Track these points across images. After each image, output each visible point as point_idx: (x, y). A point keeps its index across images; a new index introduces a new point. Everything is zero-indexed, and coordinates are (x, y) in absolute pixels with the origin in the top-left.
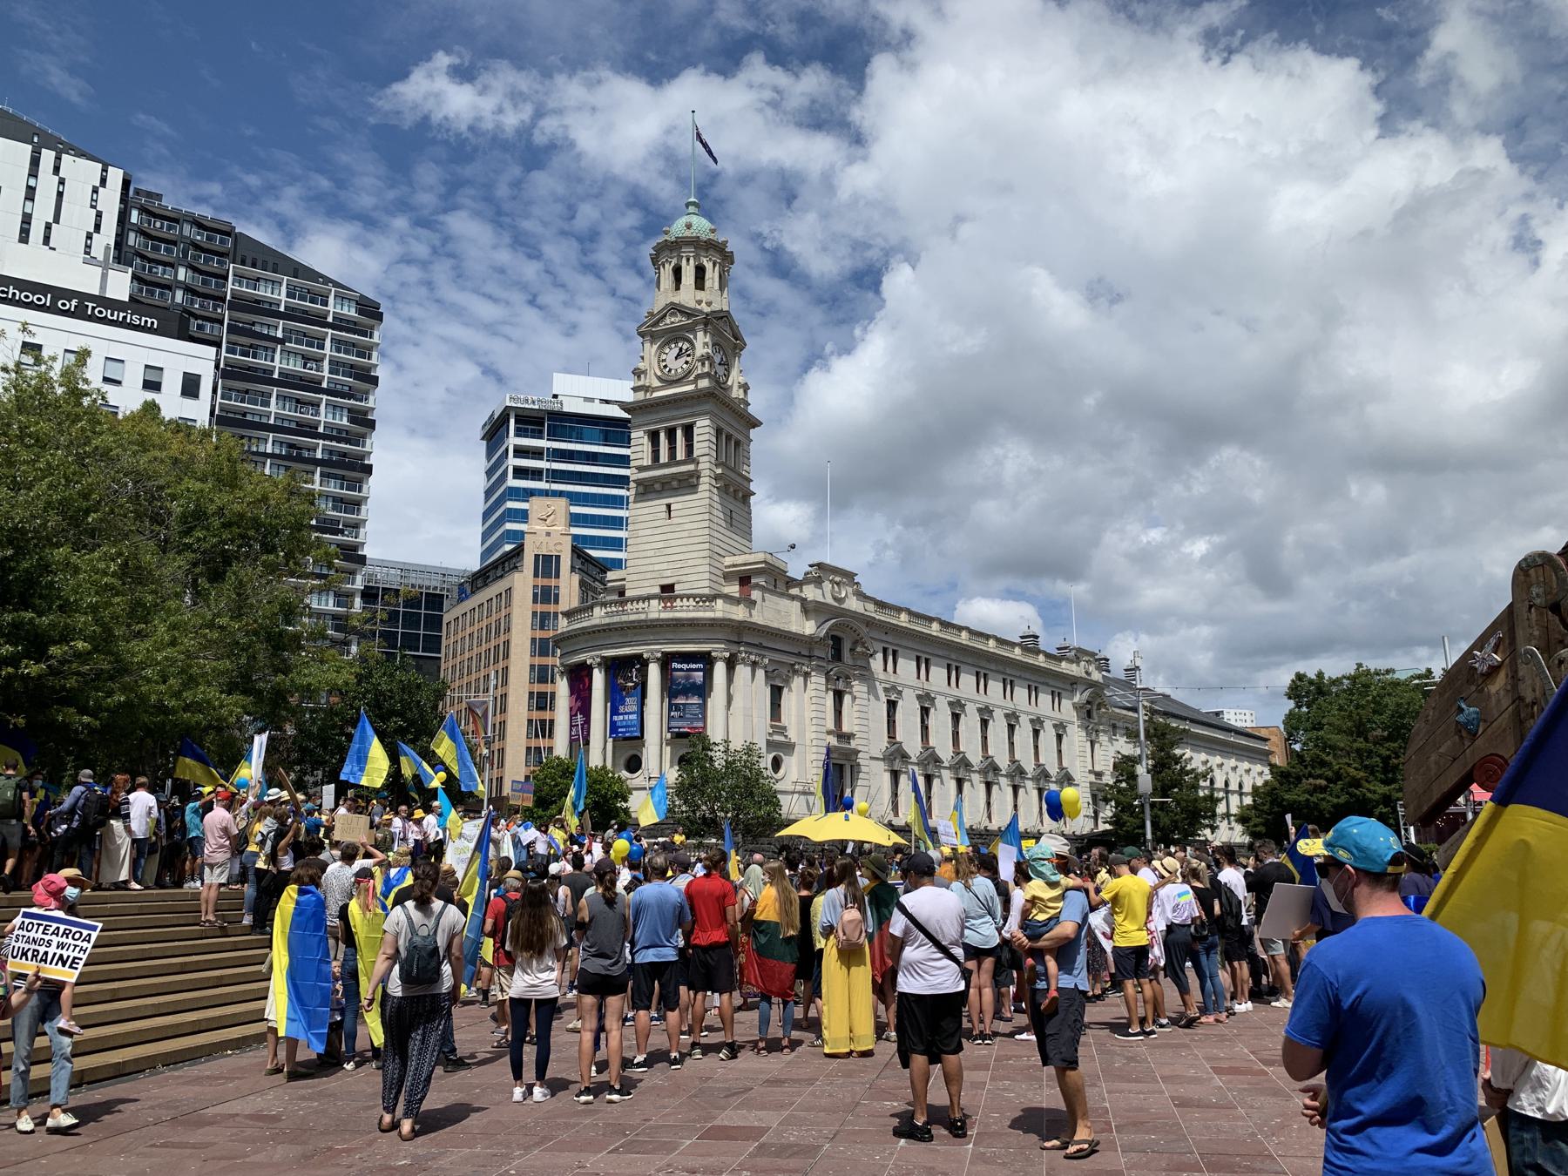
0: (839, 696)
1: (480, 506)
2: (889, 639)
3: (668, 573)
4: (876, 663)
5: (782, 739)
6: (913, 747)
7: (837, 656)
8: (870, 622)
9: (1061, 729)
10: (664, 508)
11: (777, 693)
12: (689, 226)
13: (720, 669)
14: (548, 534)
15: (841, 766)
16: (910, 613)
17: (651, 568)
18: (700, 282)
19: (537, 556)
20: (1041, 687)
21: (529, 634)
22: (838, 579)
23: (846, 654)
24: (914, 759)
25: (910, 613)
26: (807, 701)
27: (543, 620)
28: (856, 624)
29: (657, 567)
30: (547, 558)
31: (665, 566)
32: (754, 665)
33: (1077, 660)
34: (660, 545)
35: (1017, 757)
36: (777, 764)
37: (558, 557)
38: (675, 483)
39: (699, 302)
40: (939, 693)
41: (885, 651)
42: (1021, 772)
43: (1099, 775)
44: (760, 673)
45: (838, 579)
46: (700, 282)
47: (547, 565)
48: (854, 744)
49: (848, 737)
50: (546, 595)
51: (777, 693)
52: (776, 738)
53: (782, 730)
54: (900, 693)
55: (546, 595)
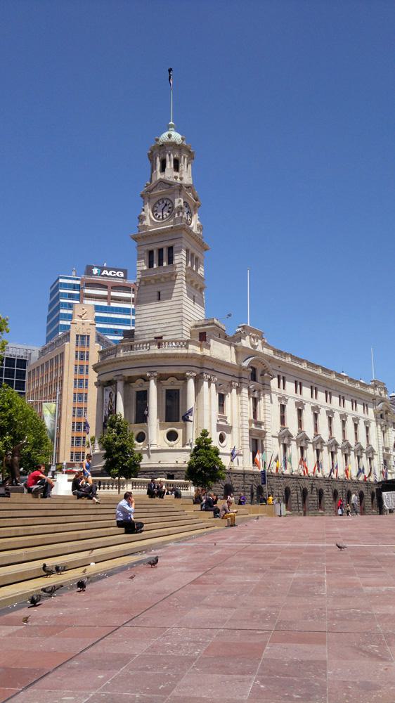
0: (255, 401)
1: (47, 313)
2: (281, 369)
3: (159, 330)
4: (274, 383)
5: (224, 424)
6: (294, 430)
7: (254, 378)
8: (271, 360)
9: (367, 423)
10: (156, 294)
11: (222, 398)
12: (170, 136)
13: (191, 383)
14: (83, 324)
15: (257, 440)
16: (293, 357)
17: (149, 327)
18: (176, 168)
19: (77, 336)
20: (358, 401)
21: (72, 390)
22: (254, 335)
23: (259, 377)
24: (295, 438)
25: (293, 357)
26: (239, 404)
27: (77, 441)
28: (265, 361)
29: (152, 327)
30: (83, 336)
31: (157, 326)
32: (210, 381)
33: (375, 387)
34: (154, 314)
35: (346, 439)
36: (222, 439)
37: (88, 336)
38: (163, 280)
39: (176, 178)
40: (308, 402)
41: (279, 377)
42: (349, 447)
43: (387, 449)
44: (213, 386)
45: (254, 335)
46: (176, 168)
47: (83, 339)
48: (263, 428)
49: (260, 424)
50: (82, 356)
51: (222, 398)
52: (221, 423)
53: (224, 419)
54: (286, 400)
55: (82, 356)
